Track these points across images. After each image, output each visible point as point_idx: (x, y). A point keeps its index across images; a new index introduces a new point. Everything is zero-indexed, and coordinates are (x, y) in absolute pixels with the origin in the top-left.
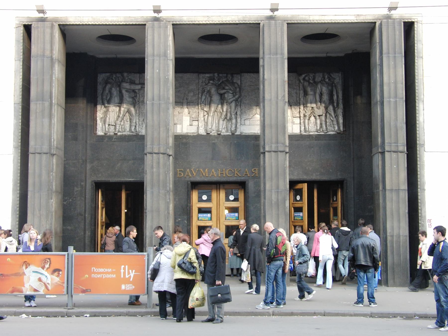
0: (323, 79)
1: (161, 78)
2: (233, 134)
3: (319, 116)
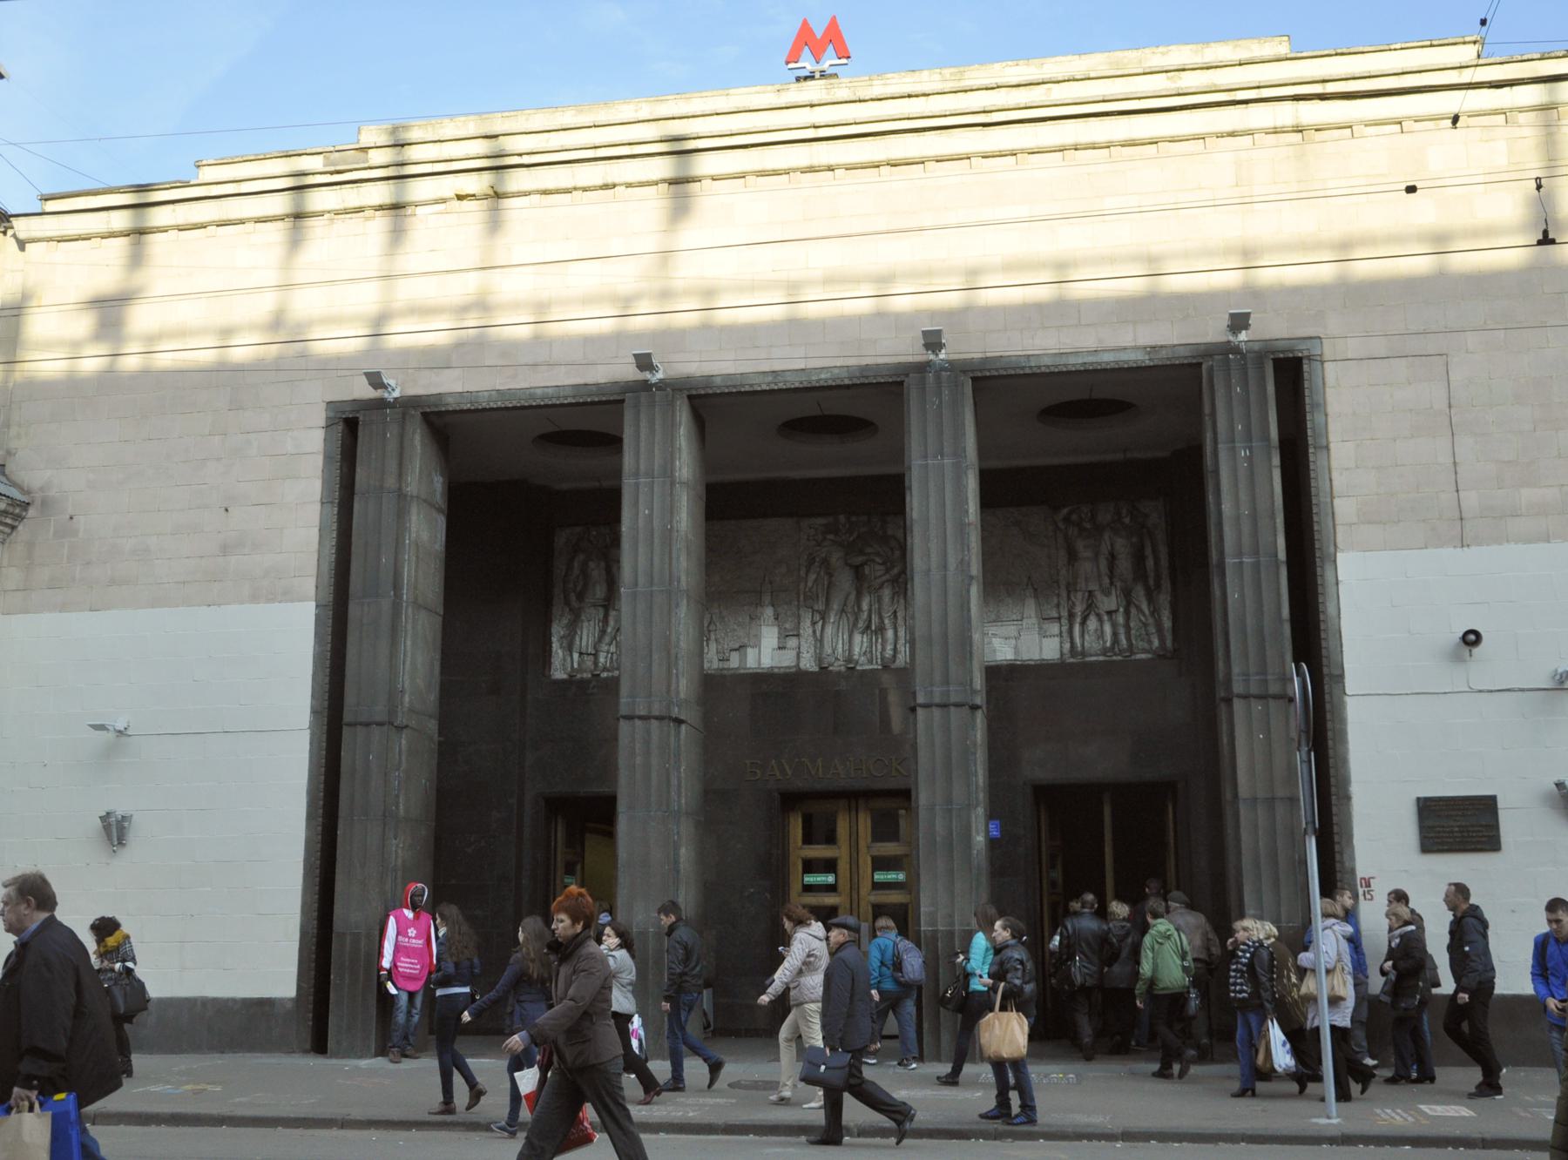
2: (885, 667)
3: (1109, 613)
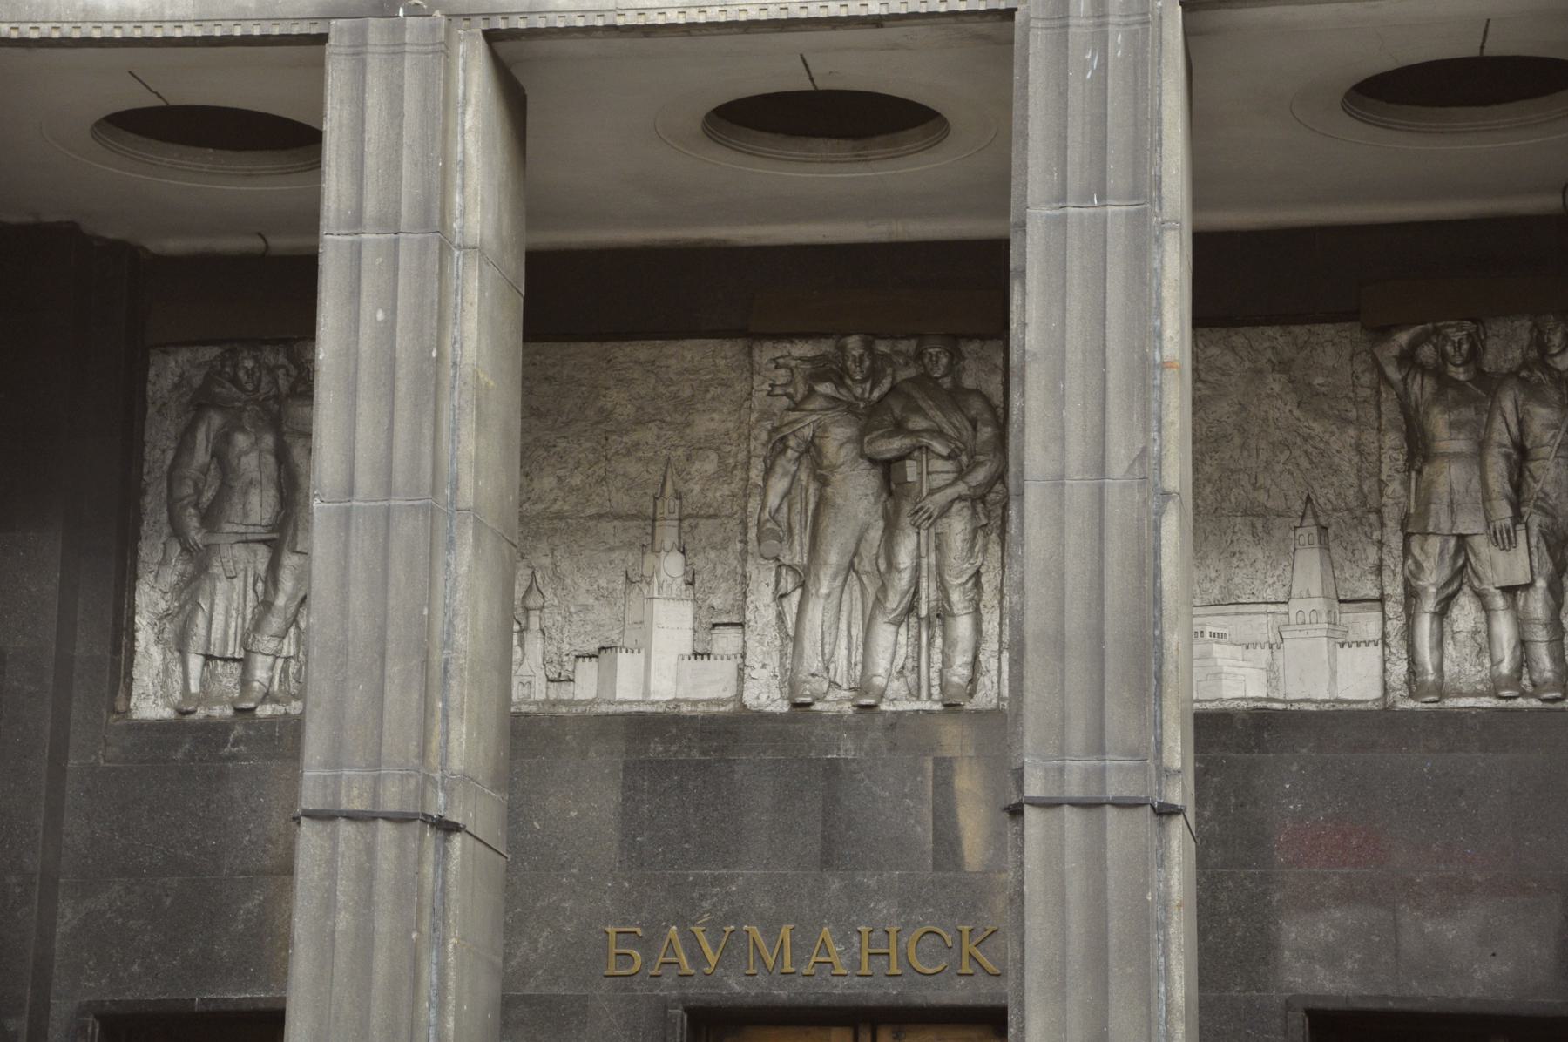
0: (1533, 354)
1: (402, 355)
3: (1510, 591)
